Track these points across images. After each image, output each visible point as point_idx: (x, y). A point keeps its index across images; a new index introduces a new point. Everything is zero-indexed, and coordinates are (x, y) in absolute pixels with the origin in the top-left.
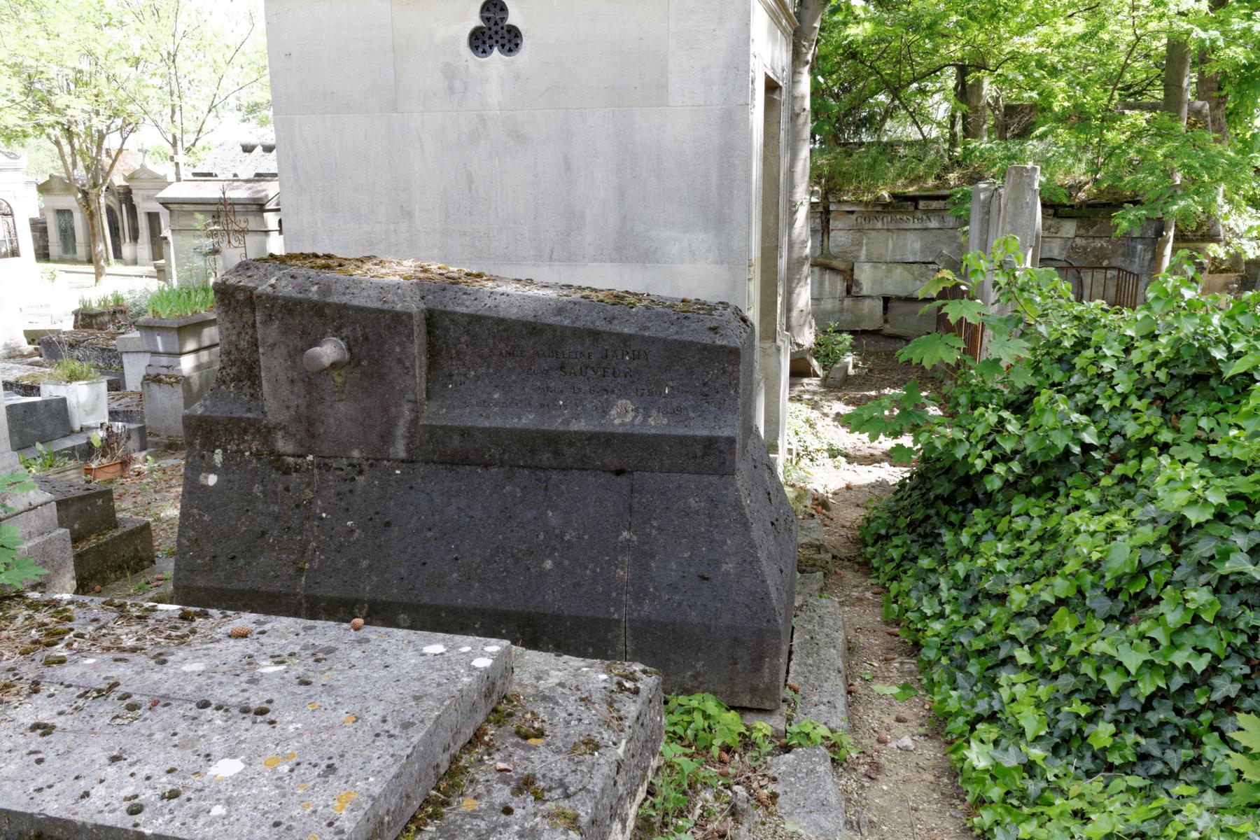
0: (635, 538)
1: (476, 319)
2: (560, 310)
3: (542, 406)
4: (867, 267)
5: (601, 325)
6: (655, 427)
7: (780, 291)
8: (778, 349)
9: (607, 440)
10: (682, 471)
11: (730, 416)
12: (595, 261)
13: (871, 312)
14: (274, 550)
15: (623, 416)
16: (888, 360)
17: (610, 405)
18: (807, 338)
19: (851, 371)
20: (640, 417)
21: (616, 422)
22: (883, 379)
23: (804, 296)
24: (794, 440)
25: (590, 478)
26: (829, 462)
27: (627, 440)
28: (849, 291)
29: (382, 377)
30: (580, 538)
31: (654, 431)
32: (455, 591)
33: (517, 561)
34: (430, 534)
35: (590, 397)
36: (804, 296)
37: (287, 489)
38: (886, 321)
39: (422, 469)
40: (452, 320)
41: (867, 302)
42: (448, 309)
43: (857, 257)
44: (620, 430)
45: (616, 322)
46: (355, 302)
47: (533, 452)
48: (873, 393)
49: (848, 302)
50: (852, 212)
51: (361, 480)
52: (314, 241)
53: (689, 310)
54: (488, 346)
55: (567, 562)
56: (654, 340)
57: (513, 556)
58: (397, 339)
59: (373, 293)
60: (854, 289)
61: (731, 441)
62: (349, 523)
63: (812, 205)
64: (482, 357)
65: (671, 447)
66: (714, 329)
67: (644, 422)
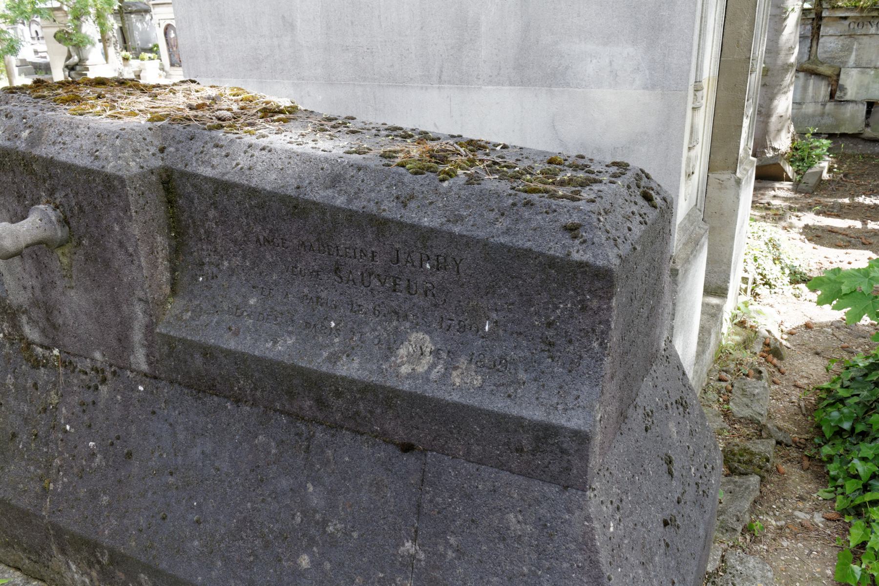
0: (422, 556)
1: (222, 187)
2: (335, 180)
3: (307, 325)
4: (854, 72)
5: (390, 210)
6: (460, 389)
7: (749, 110)
8: (738, 182)
9: (386, 398)
10: (501, 466)
11: (586, 388)
12: (490, 83)
13: (852, 117)
14: (23, 459)
15: (415, 361)
16: (864, 163)
17: (399, 338)
18: (783, 143)
19: (826, 176)
20: (440, 367)
21: (405, 370)
22: (859, 185)
23: (784, 104)
24: (751, 267)
25: (365, 448)
26: (789, 289)
27: (417, 403)
28: (832, 96)
29: (107, 264)
30: (347, 534)
31: (455, 397)
32: (195, 564)
33: (267, 545)
34: (171, 480)
35: (373, 320)
36: (784, 104)
37: (35, 385)
38: (867, 125)
39: (166, 391)
40: (194, 186)
41: (850, 107)
42: (189, 169)
43: (845, 63)
44: (406, 386)
45: (413, 205)
46: (63, 158)
47: (291, 394)
48: (847, 201)
49: (830, 106)
50: (845, 18)
51: (104, 389)
52: (207, 59)
53: (567, 174)
54: (241, 228)
55: (328, 566)
56: (468, 242)
57: (263, 536)
58: (114, 213)
59: (86, 143)
60: (838, 94)
61: (582, 438)
62: (91, 444)
63: (804, 11)
64: (235, 242)
65: (483, 427)
66: (572, 230)
67: (446, 376)
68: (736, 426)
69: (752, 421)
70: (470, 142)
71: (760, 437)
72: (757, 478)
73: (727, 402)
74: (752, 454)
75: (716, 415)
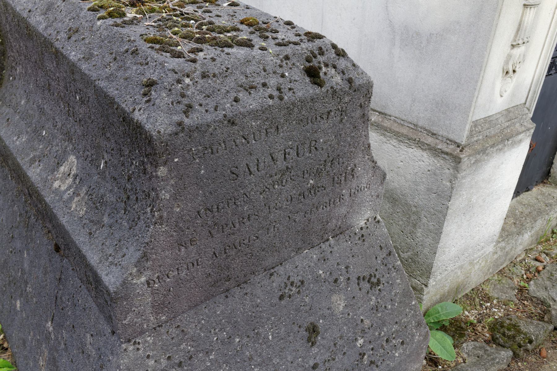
48: (270, 337)
68: (525, 302)
69: (543, 303)
70: (308, 34)
71: (541, 319)
72: (511, 353)
73: (529, 280)
74: (519, 332)
75: (511, 288)
